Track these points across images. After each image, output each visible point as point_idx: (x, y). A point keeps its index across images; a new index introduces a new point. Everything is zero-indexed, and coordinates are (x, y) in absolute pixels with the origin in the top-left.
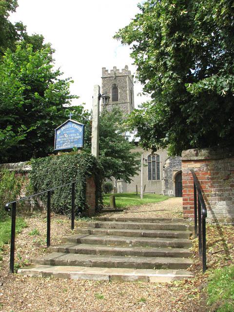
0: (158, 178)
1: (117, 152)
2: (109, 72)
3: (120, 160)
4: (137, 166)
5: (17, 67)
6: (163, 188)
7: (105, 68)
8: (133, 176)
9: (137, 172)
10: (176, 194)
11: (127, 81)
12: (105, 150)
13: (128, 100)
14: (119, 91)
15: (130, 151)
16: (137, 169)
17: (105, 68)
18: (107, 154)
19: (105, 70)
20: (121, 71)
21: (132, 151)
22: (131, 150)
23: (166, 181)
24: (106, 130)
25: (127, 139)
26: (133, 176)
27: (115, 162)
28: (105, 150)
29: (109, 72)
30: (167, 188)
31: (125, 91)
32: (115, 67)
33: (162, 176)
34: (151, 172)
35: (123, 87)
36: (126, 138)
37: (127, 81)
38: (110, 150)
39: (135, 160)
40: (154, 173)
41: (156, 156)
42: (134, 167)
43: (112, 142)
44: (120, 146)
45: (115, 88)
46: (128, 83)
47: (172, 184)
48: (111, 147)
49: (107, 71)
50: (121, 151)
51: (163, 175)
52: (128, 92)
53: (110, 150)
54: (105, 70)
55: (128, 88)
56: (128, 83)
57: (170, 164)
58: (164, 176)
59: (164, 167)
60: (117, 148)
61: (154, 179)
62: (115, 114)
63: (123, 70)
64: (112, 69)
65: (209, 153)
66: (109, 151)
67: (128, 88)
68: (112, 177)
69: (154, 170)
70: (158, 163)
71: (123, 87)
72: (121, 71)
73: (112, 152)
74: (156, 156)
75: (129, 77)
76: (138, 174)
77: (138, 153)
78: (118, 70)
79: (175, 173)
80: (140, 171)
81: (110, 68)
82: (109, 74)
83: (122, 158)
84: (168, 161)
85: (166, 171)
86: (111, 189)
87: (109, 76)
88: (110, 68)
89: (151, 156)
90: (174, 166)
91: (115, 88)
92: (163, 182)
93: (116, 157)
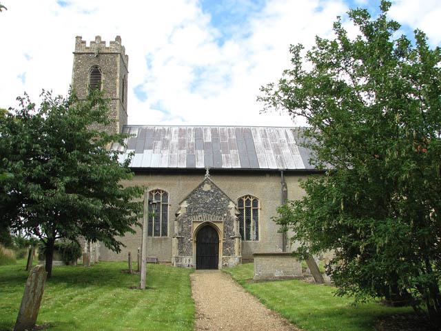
0: (165, 233)
1: (92, 183)
2: (88, 45)
3: (99, 201)
4: (133, 215)
5: (36, 181)
6: (175, 252)
7: (81, 38)
8: (122, 235)
9: (133, 227)
10: (197, 264)
11: (118, 63)
12: (67, 179)
13: (118, 96)
14: (103, 78)
15: (119, 183)
16: (134, 220)
17: (293, 60)
18: (70, 188)
19: (80, 41)
20: (108, 45)
21: (125, 183)
22: (122, 182)
23: (181, 240)
24: (71, 135)
25: (116, 158)
26: (122, 235)
27: (85, 207)
28: (67, 179)
29: (88, 45)
30: (181, 253)
31: (114, 79)
32: (98, 38)
33: (173, 229)
34: (152, 221)
35: (111, 73)
36: (113, 155)
37: (118, 63)
38: (77, 179)
39: (130, 201)
40: (157, 224)
41: (161, 194)
42: (128, 217)
43: (83, 161)
44: (98, 171)
45: (96, 73)
46: (119, 66)
47: (191, 245)
48: (82, 173)
49: (84, 42)
50: (101, 182)
51: (173, 228)
52: (118, 80)
53: (77, 179)
54: (80, 41)
55: (118, 75)
56: (119, 66)
57: (189, 209)
58: (176, 231)
59: (177, 215)
60: (94, 176)
61: (157, 234)
62: (93, 104)
63: (111, 43)
64: (94, 40)
65: (100, 240)
66: (74, 182)
67: (118, 75)
68: (80, 236)
69: (157, 218)
70: (165, 206)
71: (110, 72)
72: (108, 45)
73: (81, 184)
74: (161, 194)
75: (121, 57)
76: (134, 232)
77: (137, 188)
78: (104, 42)
79: (196, 226)
80: (141, 226)
81: (89, 38)
82: (87, 48)
83: (104, 197)
84: (185, 205)
85: (180, 223)
86: (79, 256)
87: (87, 51)
88: (89, 38)
89: (245, 200)
90: (196, 214)
91: (96, 73)
92: (175, 242)
93: (89, 195)
